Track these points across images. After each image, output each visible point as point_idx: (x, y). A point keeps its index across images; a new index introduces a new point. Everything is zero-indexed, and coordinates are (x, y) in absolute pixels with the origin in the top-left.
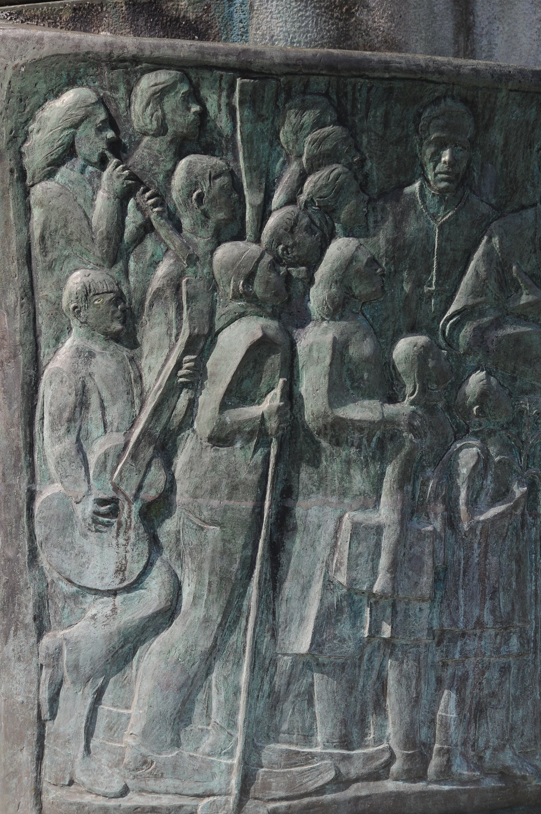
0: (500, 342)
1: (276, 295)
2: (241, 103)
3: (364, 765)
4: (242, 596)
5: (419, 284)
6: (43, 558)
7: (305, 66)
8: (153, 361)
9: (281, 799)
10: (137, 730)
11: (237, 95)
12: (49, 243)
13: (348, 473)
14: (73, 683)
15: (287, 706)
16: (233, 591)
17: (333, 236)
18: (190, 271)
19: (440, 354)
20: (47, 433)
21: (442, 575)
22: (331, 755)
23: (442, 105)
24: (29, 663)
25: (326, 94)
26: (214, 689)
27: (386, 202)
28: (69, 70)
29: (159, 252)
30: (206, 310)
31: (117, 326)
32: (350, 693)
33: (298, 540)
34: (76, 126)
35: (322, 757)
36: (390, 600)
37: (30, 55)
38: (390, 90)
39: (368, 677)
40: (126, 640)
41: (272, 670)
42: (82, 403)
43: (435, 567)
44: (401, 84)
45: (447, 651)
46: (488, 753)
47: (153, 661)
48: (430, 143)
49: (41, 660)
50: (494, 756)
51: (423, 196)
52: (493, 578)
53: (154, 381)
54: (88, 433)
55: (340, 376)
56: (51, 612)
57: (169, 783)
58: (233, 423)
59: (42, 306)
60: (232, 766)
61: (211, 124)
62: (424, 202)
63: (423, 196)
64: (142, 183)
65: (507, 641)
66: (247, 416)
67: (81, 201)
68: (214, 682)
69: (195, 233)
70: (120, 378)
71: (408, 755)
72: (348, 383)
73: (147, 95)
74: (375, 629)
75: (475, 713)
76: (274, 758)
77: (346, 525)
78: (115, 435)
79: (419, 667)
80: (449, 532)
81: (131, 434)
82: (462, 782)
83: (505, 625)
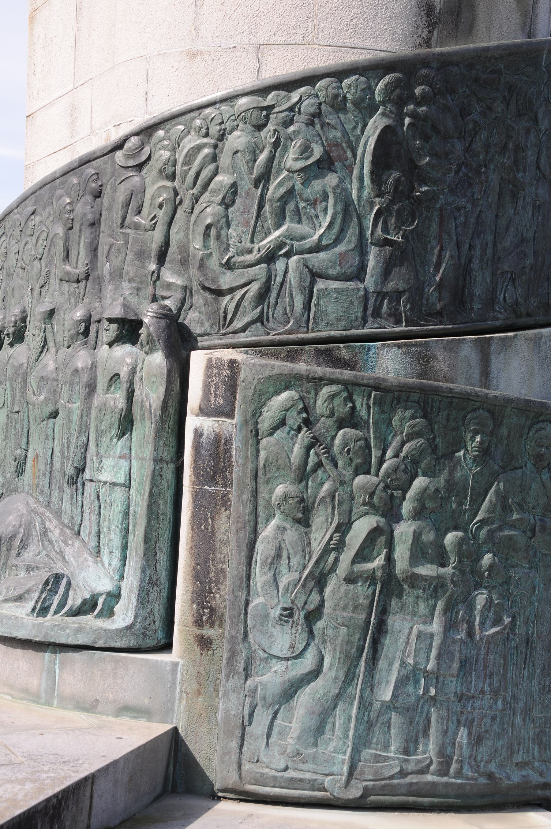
0: (501, 538)
1: (385, 504)
2: (374, 404)
3: (416, 765)
4: (356, 666)
5: (460, 504)
6: (251, 636)
7: (409, 388)
8: (317, 535)
9: (370, 780)
10: (295, 735)
11: (372, 399)
12: (267, 469)
13: (417, 603)
14: (262, 706)
15: (376, 729)
16: (351, 663)
17: (416, 475)
18: (341, 489)
19: (469, 543)
20: (258, 570)
21: (463, 663)
22: (398, 758)
23: (478, 412)
24: (239, 693)
25: (418, 402)
26: (337, 716)
27: (445, 460)
28: (286, 382)
29: (325, 478)
30: (347, 510)
31: (300, 515)
32: (411, 725)
33: (388, 638)
34: (287, 410)
35: (394, 759)
36: (436, 675)
37: (267, 373)
38: (451, 403)
39: (420, 716)
40: (292, 686)
41: (369, 709)
42: (278, 555)
43: (460, 658)
44: (457, 400)
45: (464, 706)
46: (482, 764)
47: (306, 698)
48: (470, 431)
49: (246, 693)
50: (485, 766)
51: (465, 458)
52: (491, 667)
53: (317, 546)
54: (280, 571)
55: (416, 551)
56: (253, 667)
57: (310, 766)
58: (358, 572)
59: (261, 502)
60: (345, 760)
61: (357, 413)
62: (465, 462)
63: (465, 458)
64: (319, 441)
65: (496, 703)
66: (366, 569)
67: (286, 448)
68: (338, 713)
69: (345, 469)
70: (299, 543)
71: (440, 762)
72: (420, 554)
73: (326, 397)
74: (426, 690)
75: (477, 741)
76: (368, 757)
77: (415, 632)
78: (294, 573)
79: (448, 713)
80: (469, 640)
81: (303, 573)
82: (468, 779)
83: (496, 693)
